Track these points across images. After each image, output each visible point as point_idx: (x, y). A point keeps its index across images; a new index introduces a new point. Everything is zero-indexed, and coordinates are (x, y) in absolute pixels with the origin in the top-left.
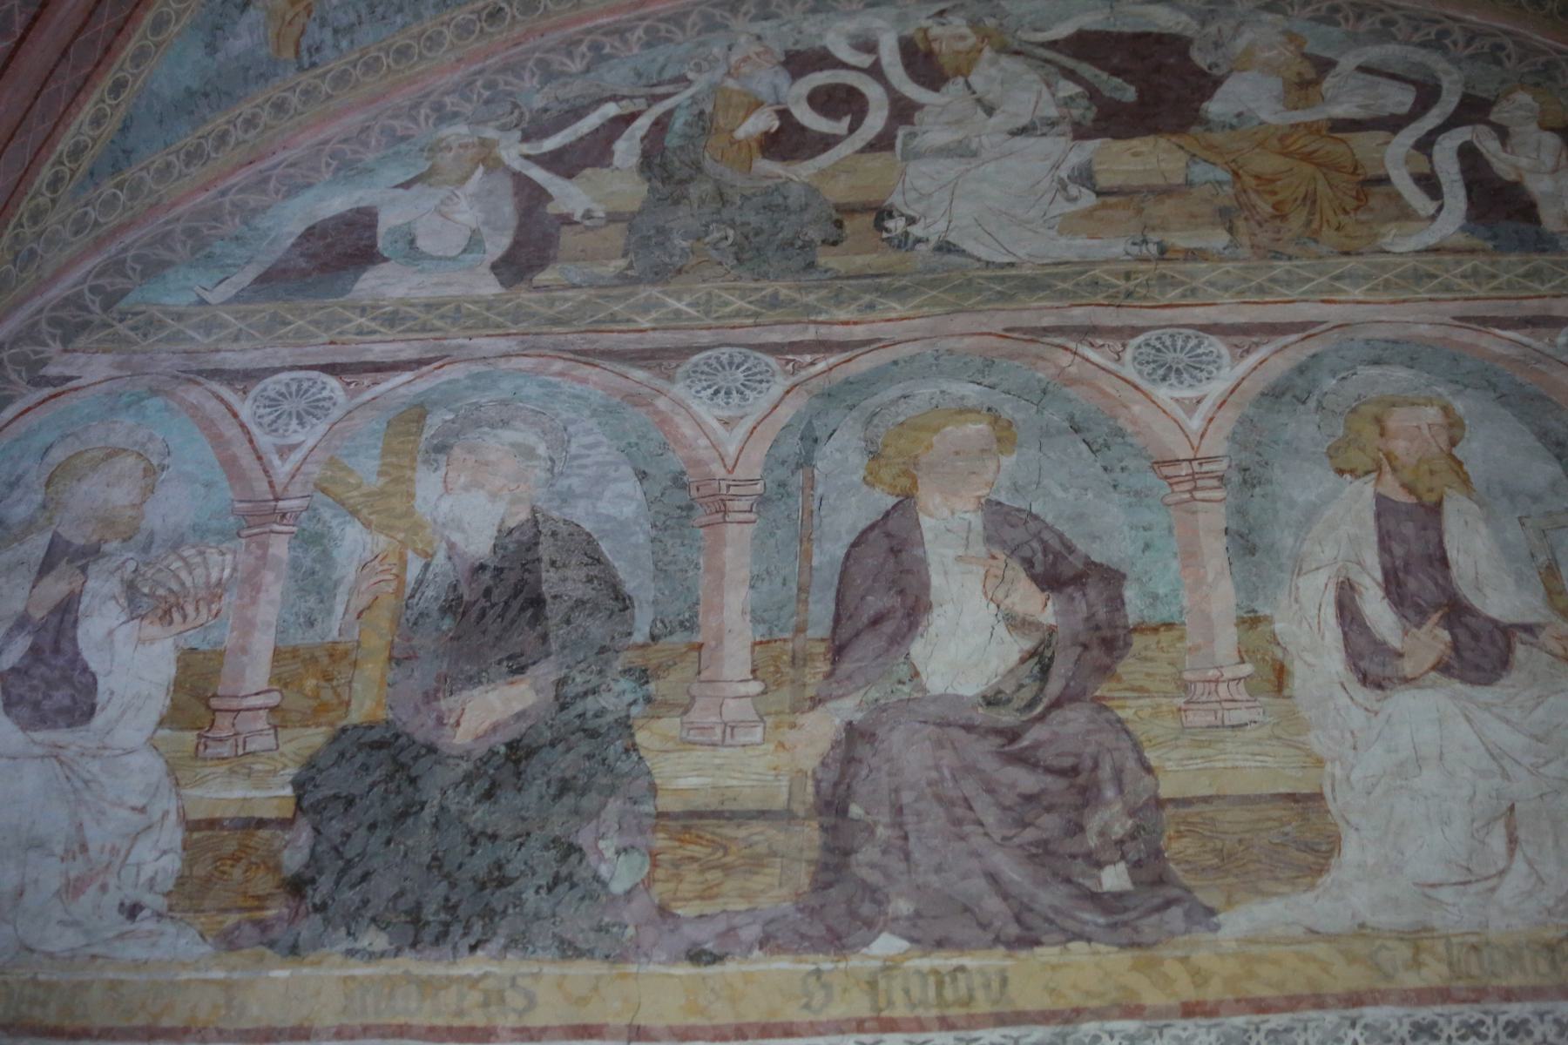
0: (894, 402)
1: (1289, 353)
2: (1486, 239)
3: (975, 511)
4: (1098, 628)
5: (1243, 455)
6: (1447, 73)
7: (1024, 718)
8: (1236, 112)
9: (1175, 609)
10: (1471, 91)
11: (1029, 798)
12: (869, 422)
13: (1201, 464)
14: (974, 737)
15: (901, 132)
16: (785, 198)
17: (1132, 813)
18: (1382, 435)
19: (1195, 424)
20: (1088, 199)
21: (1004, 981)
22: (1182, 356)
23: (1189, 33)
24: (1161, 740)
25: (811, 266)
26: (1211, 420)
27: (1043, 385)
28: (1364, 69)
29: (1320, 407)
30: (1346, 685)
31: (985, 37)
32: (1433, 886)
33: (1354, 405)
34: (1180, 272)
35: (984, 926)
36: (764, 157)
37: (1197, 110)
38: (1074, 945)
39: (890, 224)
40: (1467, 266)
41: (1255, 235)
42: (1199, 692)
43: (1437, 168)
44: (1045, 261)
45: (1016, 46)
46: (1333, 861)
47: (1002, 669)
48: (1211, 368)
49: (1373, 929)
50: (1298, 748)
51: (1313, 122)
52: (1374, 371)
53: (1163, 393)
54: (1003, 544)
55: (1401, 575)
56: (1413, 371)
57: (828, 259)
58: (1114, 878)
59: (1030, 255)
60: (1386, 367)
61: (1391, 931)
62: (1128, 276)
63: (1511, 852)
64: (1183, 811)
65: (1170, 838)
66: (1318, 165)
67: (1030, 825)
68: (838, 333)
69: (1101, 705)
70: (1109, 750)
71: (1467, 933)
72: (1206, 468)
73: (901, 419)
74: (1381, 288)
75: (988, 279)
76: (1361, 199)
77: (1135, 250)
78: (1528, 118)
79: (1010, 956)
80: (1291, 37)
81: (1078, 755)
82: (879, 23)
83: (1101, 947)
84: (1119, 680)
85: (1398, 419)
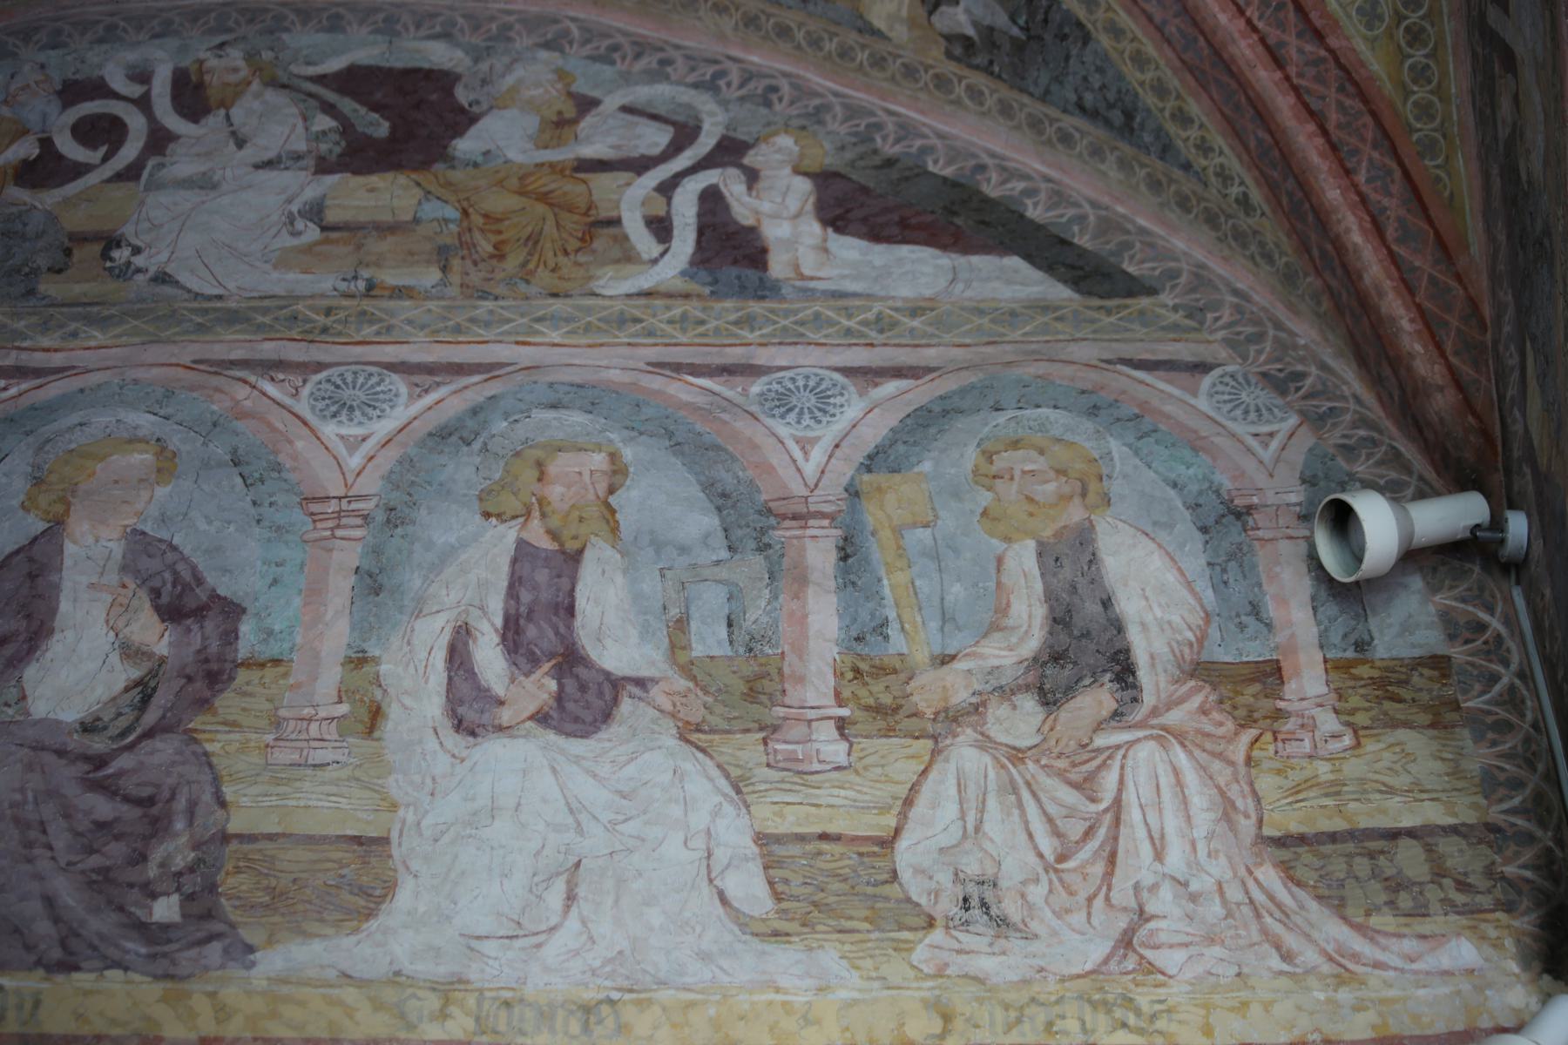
0: (70, 429)
1: (469, 394)
2: (704, 284)
3: (119, 540)
4: (207, 661)
5: (395, 494)
6: (711, 114)
7: (115, 747)
8: (484, 150)
9: (286, 645)
10: (731, 134)
11: (101, 826)
12: (40, 449)
13: (349, 502)
14: (63, 762)
15: (151, 163)
16: (25, 225)
17: (196, 846)
18: (540, 480)
19: (355, 462)
20: (312, 233)
21: (37, 1004)
22: (357, 392)
23: (459, 70)
24: (241, 775)
25: (31, 292)
26: (372, 458)
27: (215, 418)
28: (627, 109)
29: (485, 448)
30: (439, 730)
31: (257, 68)
32: (479, 938)
33: (519, 448)
34: (380, 310)
35: (28, 948)
36: (16, 184)
37: (445, 147)
38: (109, 973)
39: (116, 254)
40: (677, 312)
41: (467, 274)
42: (290, 729)
43: (673, 211)
44: (252, 295)
45: (285, 80)
46: (383, 907)
47: (105, 698)
48: (385, 406)
49: (408, 977)
50: (376, 791)
51: (559, 162)
52: (550, 415)
53: (329, 430)
54: (136, 573)
55: (522, 622)
56: (590, 416)
57: (50, 287)
58: (166, 909)
59: (238, 288)
60: (563, 411)
61: (425, 981)
62: (328, 312)
63: (567, 908)
64: (246, 847)
65: (227, 874)
66: (551, 205)
67: (97, 851)
68: (38, 359)
69: (191, 738)
70: (189, 783)
71: (502, 988)
72: (354, 506)
73: (73, 446)
74: (581, 331)
75: (192, 310)
76: (586, 239)
77: (343, 286)
78: (784, 161)
79: (46, 979)
80: (561, 74)
81: (158, 786)
82: (160, 54)
83: (137, 977)
84: (215, 714)
85: (561, 465)
